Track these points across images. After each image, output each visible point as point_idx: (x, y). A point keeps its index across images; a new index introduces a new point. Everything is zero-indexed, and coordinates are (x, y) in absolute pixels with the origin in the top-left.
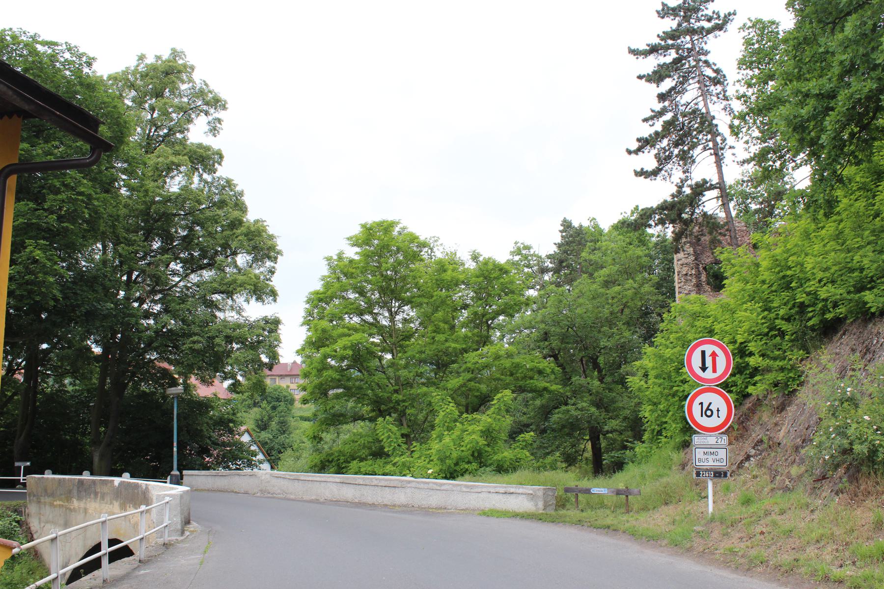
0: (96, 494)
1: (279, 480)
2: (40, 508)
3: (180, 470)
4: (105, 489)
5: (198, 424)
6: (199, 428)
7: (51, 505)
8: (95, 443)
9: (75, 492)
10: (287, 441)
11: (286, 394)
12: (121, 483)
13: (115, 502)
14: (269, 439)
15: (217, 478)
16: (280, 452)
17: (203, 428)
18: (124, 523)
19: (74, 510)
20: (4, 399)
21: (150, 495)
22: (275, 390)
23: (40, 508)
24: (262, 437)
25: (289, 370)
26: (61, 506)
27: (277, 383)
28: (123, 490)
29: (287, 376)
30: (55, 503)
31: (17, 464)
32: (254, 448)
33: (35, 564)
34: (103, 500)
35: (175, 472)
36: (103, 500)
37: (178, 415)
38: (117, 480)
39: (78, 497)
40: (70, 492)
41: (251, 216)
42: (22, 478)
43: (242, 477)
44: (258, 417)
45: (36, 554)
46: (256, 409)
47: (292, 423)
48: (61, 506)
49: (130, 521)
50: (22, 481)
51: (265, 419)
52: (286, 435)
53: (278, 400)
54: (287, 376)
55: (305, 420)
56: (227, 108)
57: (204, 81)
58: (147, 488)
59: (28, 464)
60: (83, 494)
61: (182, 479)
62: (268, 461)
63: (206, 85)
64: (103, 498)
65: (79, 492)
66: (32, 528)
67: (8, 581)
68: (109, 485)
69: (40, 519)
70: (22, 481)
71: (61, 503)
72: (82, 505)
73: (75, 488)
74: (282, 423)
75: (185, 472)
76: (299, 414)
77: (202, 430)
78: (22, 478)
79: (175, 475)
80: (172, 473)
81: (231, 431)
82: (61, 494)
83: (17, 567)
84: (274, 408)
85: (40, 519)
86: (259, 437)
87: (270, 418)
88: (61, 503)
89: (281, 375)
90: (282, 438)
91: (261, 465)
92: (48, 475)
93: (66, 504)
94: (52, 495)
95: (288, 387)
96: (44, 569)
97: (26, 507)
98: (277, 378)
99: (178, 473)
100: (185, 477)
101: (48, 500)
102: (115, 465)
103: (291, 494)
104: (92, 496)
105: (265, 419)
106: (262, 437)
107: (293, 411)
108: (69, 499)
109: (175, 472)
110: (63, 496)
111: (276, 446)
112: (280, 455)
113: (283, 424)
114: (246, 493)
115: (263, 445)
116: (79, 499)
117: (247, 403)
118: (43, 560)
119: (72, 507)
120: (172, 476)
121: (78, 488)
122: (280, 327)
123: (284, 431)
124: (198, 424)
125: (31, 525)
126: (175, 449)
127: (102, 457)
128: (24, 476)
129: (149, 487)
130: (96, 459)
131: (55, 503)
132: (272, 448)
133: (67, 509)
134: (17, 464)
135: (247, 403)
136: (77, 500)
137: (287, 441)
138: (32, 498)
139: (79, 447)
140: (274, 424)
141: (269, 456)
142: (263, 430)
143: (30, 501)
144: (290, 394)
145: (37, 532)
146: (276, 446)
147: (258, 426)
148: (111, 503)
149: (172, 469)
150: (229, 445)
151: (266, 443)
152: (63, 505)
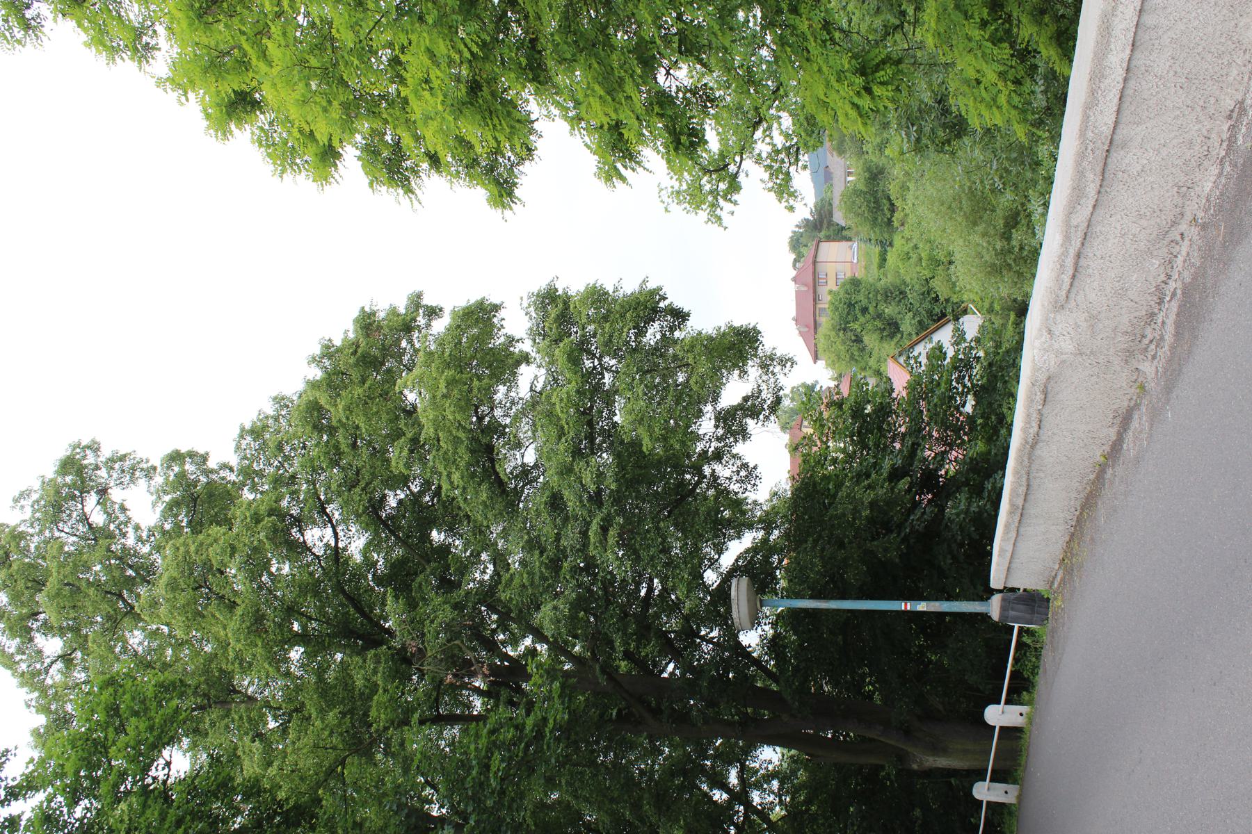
1: (1092, 263)
5: (855, 511)
6: (866, 513)
10: (917, 287)
14: (913, 318)
16: (936, 299)
22: (837, 309)
24: (910, 329)
25: (805, 289)
27: (827, 306)
29: (815, 292)
32: (922, 350)
41: (316, 373)
43: (1045, 434)
44: (876, 336)
46: (866, 339)
47: (888, 280)
51: (880, 325)
52: (907, 290)
53: (851, 305)
54: (815, 292)
55: (885, 260)
56: (94, 442)
57: (16, 500)
61: (1013, 590)
62: (957, 319)
63: (24, 494)
74: (887, 296)
76: (876, 270)
77: (873, 504)
79: (1004, 609)
81: (884, 411)
84: (865, 310)
86: (910, 334)
87: (879, 316)
89: (815, 300)
90: (912, 297)
91: (969, 337)
98: (819, 306)
103: (1185, 190)
105: (880, 325)
106: (910, 329)
107: (870, 280)
111: (926, 305)
112: (942, 299)
113: (888, 295)
115: (925, 329)
117: (856, 353)
122: (560, 288)
123: (901, 293)
124: (855, 511)
126: (922, 606)
132: (930, 313)
135: (856, 353)
137: (917, 287)
140: (889, 310)
141: (944, 315)
142: (898, 328)
144: (844, 285)
146: (926, 305)
147: (892, 336)
149: (985, 617)
150: (916, 417)
151: (920, 322)
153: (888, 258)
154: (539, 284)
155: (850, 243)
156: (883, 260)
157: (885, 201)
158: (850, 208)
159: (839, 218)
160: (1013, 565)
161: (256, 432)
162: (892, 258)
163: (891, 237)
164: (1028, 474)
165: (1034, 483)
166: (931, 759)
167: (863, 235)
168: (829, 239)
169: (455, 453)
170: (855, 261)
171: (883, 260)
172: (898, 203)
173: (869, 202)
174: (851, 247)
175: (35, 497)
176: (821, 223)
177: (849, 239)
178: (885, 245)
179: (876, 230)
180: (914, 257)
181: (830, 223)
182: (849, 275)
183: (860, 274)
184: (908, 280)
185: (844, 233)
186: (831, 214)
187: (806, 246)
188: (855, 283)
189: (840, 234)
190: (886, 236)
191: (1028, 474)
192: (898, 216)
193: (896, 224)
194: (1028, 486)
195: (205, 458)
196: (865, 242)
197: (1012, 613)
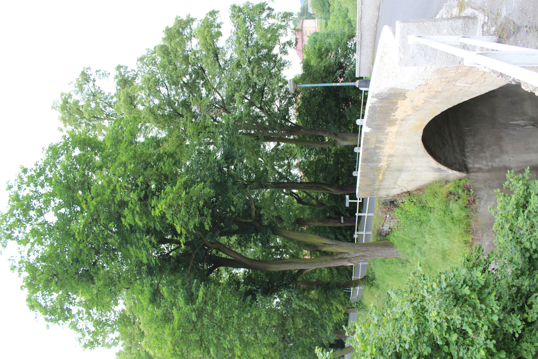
0: (376, 148)
2: (383, 188)
3: (354, 80)
4: (373, 140)
5: (320, 70)
7: (382, 181)
8: (334, 144)
9: (372, 165)
11: (312, 37)
12: (368, 125)
13: (386, 131)
15: (363, 44)
17: (323, 65)
18: (409, 122)
19: (389, 166)
20: (309, 197)
21: (385, 91)
23: (383, 188)
26: (384, 174)
28: (376, 123)
29: (302, 38)
30: (381, 178)
31: (347, 205)
33: (428, 191)
34: (383, 141)
35: (357, 84)
36: (383, 141)
37: (312, 82)
38: (365, 130)
39: (377, 162)
40: (372, 168)
42: (358, 201)
45: (420, 190)
48: (384, 174)
49: (409, 115)
50: (361, 201)
54: (302, 38)
58: (376, 96)
59: (347, 197)
60: (375, 158)
64: (381, 142)
65: (373, 162)
66: (399, 193)
67: (442, 213)
68: (368, 137)
69: (392, 188)
70: (361, 201)
71: (381, 175)
72: (385, 159)
73: (369, 164)
75: (357, 76)
77: (325, 67)
78: (358, 201)
79: (359, 83)
80: (357, 86)
82: (374, 175)
83: (430, 205)
85: (392, 188)
88: (381, 175)
89: (302, 41)
92: (358, 174)
93: (382, 171)
94: (374, 181)
95: (308, 36)
96: (433, 184)
97: (381, 197)
98: (304, 43)
99: (357, 82)
100: (361, 76)
101: (377, 183)
102: (351, 130)
104: (378, 151)
108: (378, 169)
109: (357, 84)
110: (376, 173)
114: (379, 8)
116: (379, 161)
118: (425, 185)
119: (386, 166)
120: (360, 86)
121: (369, 162)
125: (396, 193)
127: (344, 139)
128: (357, 199)
129: (376, 93)
130: (346, 143)
131: (381, 178)
133: (386, 170)
134: (347, 205)
136: (380, 163)
138: (374, 194)
139: (338, 152)
143: (376, 195)
144: (312, 35)
145: (402, 190)
148: (387, 134)
152: (383, 173)
153: (328, 23)
154: (232, 4)
155: (314, 20)
156: (326, 24)
157: (327, 3)
158: (314, 6)
159: (310, 10)
160: (361, 67)
161: (141, 59)
162: (329, 23)
163: (329, 17)
164: (361, 29)
165: (363, 35)
166: (343, 142)
167: (319, 16)
168: (307, 19)
169: (208, 54)
170: (316, 26)
171: (326, 24)
172: (331, 3)
173: (321, 3)
174: (315, 21)
175: (74, 83)
176: (304, 13)
177: (314, 18)
178: (327, 19)
179: (324, 14)
180: (337, 21)
181: (307, 13)
182: (314, 31)
183: (318, 31)
184: (335, 30)
185: (312, 16)
186: (307, 9)
187: (298, 22)
188: (316, 33)
189: (311, 17)
190: (327, 16)
191: (361, 29)
192: (331, 8)
193: (331, 11)
194: (361, 34)
195: (127, 68)
196: (320, 19)
197: (362, 84)
